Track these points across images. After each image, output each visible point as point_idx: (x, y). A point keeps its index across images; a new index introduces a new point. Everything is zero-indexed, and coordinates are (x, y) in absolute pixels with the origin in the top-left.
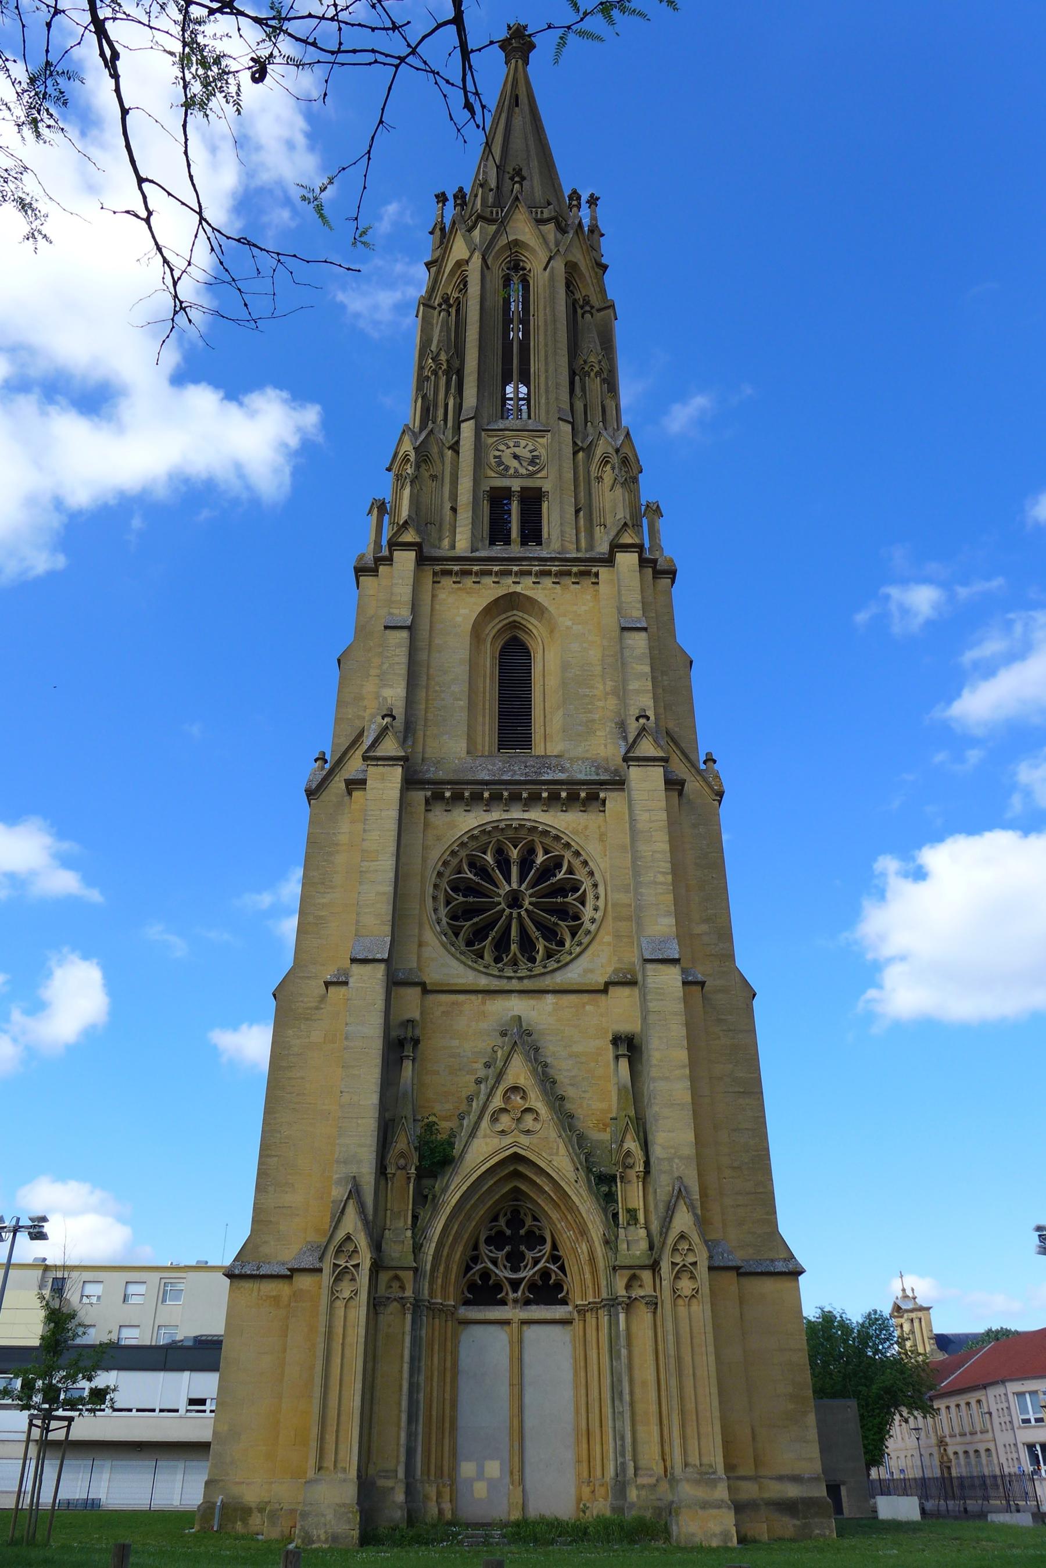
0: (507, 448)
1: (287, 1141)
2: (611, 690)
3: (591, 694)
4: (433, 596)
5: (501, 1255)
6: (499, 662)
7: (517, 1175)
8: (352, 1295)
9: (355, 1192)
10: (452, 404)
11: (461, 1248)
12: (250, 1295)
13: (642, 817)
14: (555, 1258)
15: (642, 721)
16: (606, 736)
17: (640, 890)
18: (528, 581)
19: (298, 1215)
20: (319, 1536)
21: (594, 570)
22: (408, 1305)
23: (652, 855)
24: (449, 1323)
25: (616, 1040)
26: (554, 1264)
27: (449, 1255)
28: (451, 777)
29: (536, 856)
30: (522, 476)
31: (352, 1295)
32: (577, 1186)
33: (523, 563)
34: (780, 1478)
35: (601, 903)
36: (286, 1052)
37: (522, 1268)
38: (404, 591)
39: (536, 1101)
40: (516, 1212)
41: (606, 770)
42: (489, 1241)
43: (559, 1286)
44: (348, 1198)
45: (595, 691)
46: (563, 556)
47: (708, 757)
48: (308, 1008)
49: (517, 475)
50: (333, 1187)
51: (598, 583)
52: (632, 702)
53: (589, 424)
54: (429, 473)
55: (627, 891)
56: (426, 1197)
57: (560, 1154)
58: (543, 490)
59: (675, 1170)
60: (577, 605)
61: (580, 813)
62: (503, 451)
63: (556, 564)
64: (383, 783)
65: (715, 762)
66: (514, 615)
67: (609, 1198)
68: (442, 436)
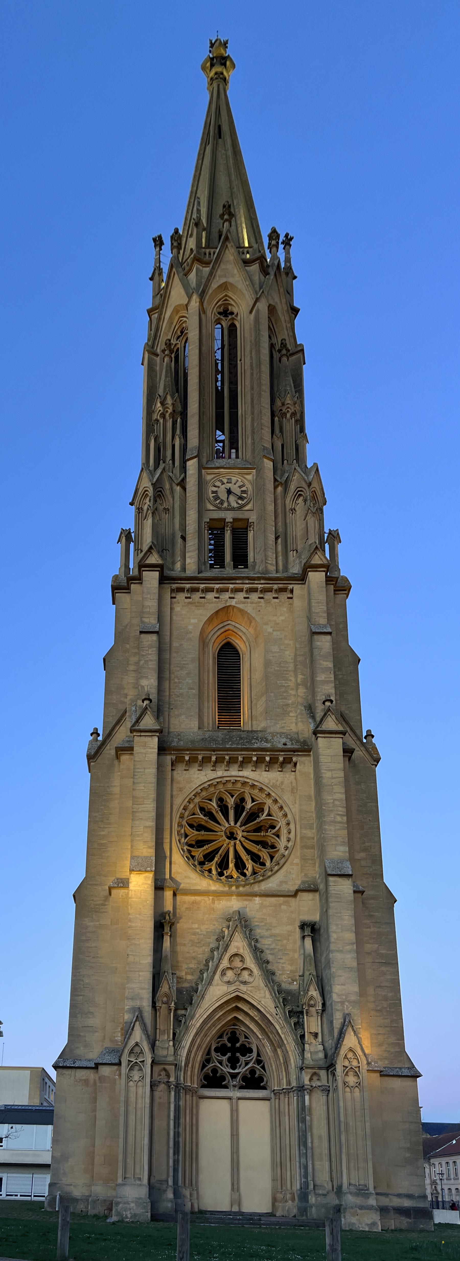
0: (222, 484)
1: (88, 986)
2: (301, 682)
3: (286, 685)
4: (171, 609)
5: (225, 1058)
6: (218, 661)
7: (237, 1009)
8: (140, 1079)
9: (140, 1017)
10: (179, 445)
11: (201, 1054)
12: (69, 1078)
13: (327, 775)
14: (259, 1062)
15: (328, 704)
16: (297, 716)
17: (324, 827)
18: (240, 596)
19: (97, 1031)
20: (126, 1215)
21: (290, 587)
22: (172, 1086)
23: (333, 802)
24: (194, 1098)
25: (303, 926)
26: (258, 1065)
27: (194, 1057)
28: (190, 746)
29: (246, 803)
30: (233, 509)
31: (140, 1079)
32: (278, 1017)
33: (237, 582)
34: (399, 1196)
35: (292, 836)
36: (84, 931)
37: (238, 1067)
38: (152, 604)
39: (250, 962)
40: (234, 1033)
41: (298, 741)
42: (216, 1050)
43: (261, 1079)
44: (136, 1021)
45: (289, 682)
46: (267, 576)
47: (369, 734)
48: (97, 905)
49: (230, 509)
50: (125, 1014)
51: (291, 598)
52: (319, 690)
53: (285, 462)
54: (163, 507)
55: (311, 828)
56: (181, 1021)
57: (267, 997)
58: (250, 521)
59: (345, 1009)
60: (276, 615)
61: (278, 773)
62: (219, 487)
63: (262, 582)
64: (145, 749)
65: (373, 736)
66: (229, 624)
67: (299, 1025)
68: (171, 474)
